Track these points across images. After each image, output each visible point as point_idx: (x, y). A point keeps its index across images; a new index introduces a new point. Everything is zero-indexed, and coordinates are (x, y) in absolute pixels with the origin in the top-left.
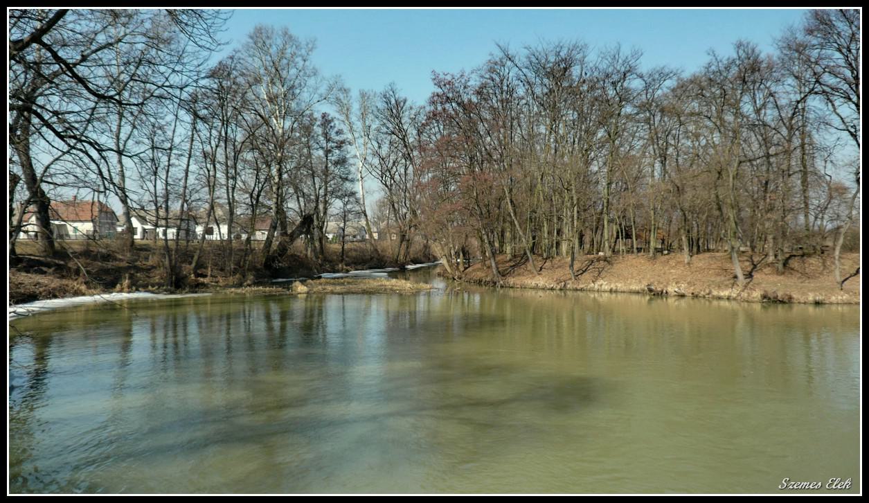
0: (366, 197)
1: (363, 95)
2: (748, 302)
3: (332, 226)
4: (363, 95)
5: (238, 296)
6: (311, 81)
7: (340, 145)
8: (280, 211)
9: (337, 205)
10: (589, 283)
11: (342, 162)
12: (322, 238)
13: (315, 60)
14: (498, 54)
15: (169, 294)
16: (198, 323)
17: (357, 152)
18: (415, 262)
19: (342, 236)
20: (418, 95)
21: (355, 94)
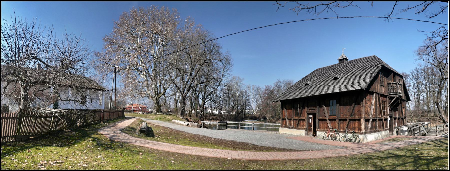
0: (254, 106)
1: (253, 86)
2: (76, 101)
3: (247, 111)
4: (253, 86)
5: (40, 148)
6: (244, 86)
7: (249, 96)
8: (238, 109)
9: (248, 107)
10: (49, 106)
11: (249, 100)
12: (245, 114)
13: (244, 82)
14: (278, 81)
15: (306, 160)
16: (225, 146)
17: (252, 97)
18: (263, 118)
19: (248, 113)
20: (263, 88)
21: (251, 86)
